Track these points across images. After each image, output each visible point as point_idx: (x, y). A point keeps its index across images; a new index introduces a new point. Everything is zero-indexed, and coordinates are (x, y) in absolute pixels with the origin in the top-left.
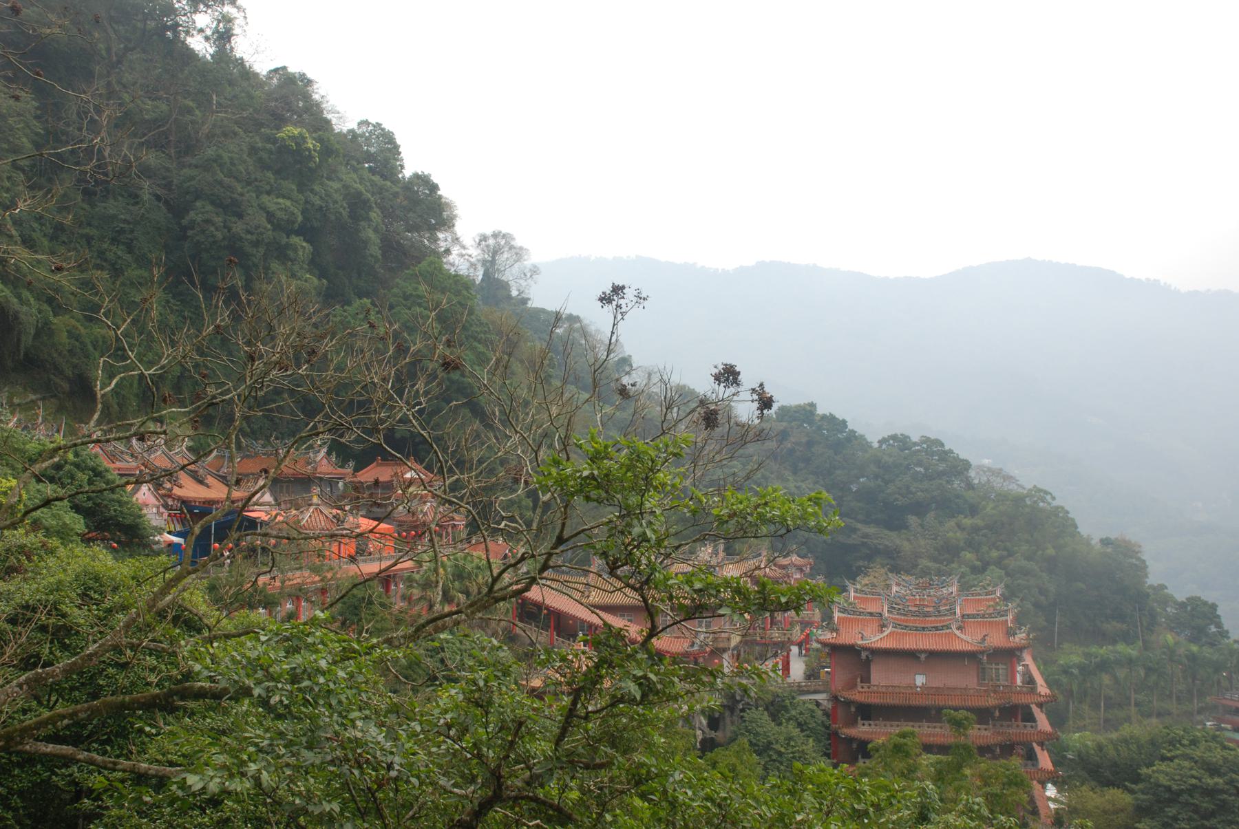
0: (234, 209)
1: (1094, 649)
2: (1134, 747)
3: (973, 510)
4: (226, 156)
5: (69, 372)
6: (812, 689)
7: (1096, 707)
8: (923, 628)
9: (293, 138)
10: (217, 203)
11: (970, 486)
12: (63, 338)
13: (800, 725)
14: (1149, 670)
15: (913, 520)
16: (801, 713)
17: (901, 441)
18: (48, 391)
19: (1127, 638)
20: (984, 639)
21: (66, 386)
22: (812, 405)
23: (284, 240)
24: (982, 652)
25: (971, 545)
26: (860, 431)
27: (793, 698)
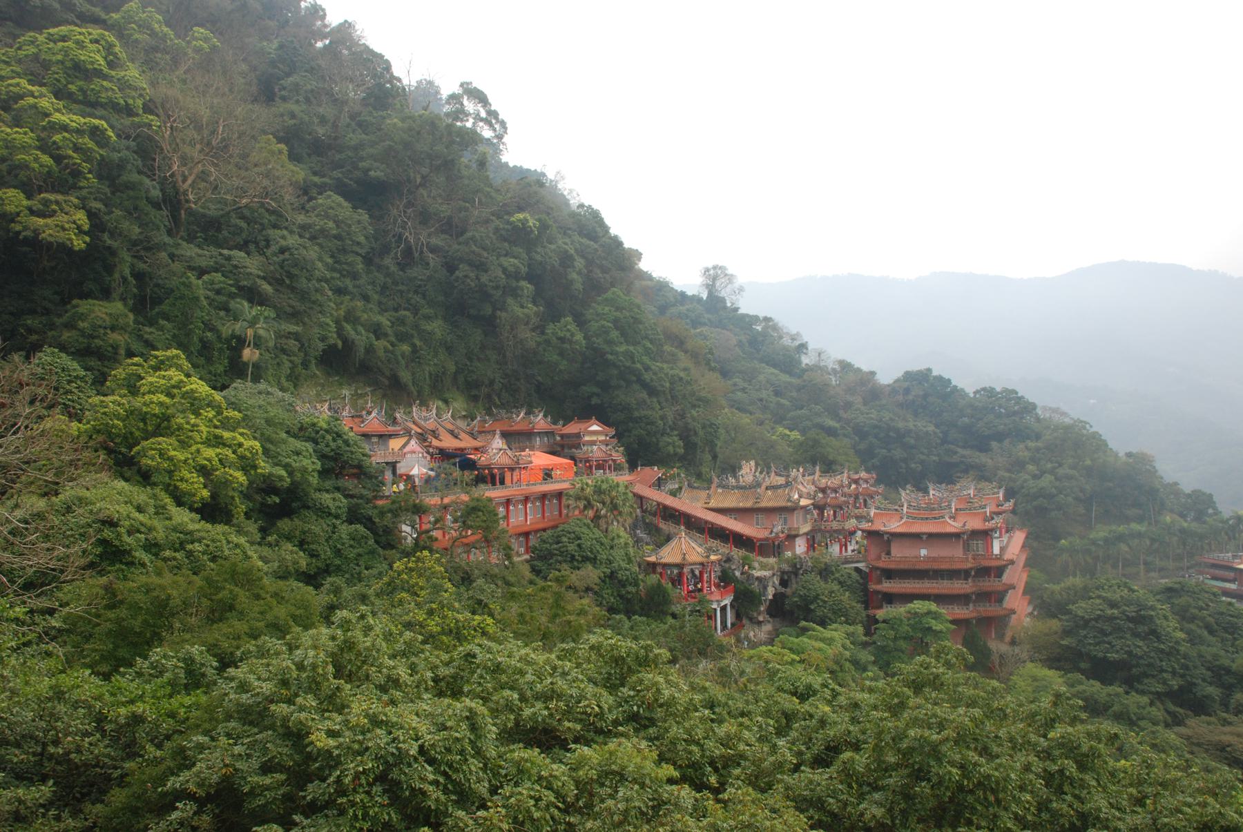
0: (481, 267)
1: (1114, 527)
2: (1072, 592)
3: (1038, 437)
4: (477, 235)
5: (388, 373)
7: (1115, 566)
9: (519, 220)
10: (471, 264)
11: (1038, 419)
12: (381, 353)
13: (840, 583)
14: (1153, 540)
15: (994, 444)
17: (989, 392)
18: (375, 384)
19: (1140, 519)
21: (387, 382)
22: (929, 370)
23: (514, 284)
25: (1034, 460)
26: (960, 386)
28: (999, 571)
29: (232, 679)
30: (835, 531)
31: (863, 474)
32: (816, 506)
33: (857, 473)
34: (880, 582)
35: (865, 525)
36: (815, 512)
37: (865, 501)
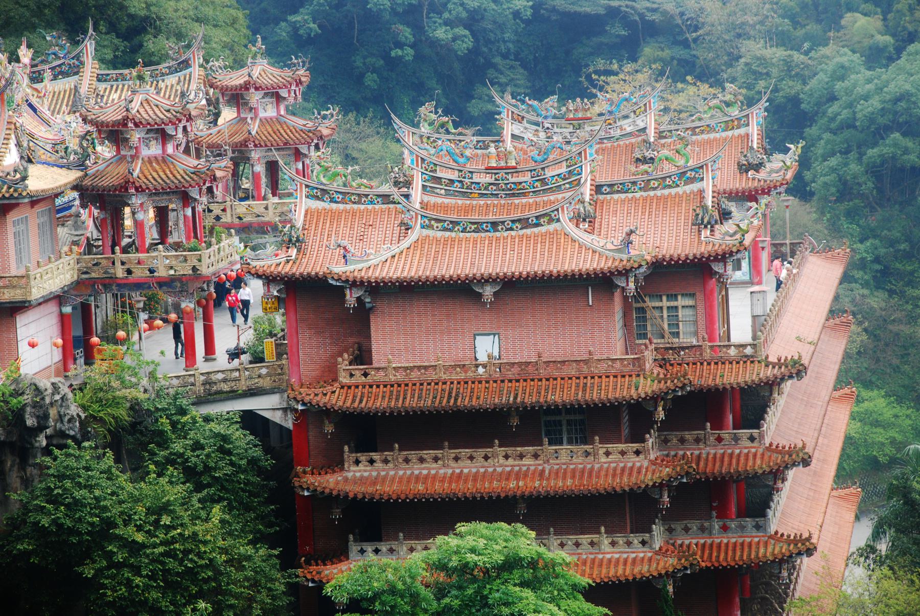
6: (243, 386)
8: (494, 225)
13: (191, 474)
16: (197, 446)
20: (628, 243)
24: (625, 273)
27: (183, 412)
28: (752, 404)
29: (190, 439)
30: (166, 284)
31: (262, 70)
32: (89, 194)
33: (238, 64)
34: (335, 463)
35: (273, 258)
36: (89, 217)
37: (273, 168)
